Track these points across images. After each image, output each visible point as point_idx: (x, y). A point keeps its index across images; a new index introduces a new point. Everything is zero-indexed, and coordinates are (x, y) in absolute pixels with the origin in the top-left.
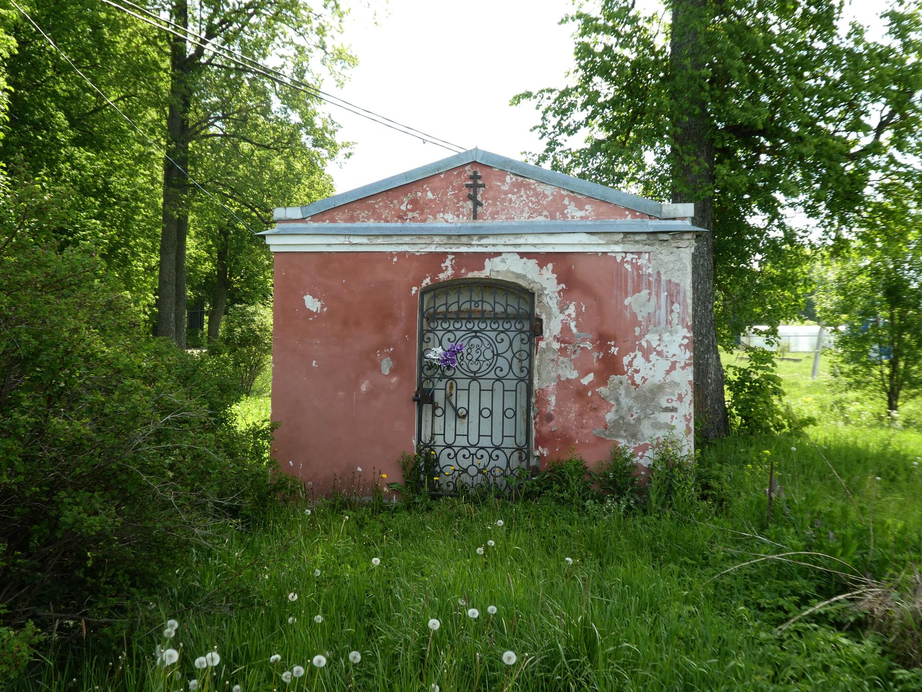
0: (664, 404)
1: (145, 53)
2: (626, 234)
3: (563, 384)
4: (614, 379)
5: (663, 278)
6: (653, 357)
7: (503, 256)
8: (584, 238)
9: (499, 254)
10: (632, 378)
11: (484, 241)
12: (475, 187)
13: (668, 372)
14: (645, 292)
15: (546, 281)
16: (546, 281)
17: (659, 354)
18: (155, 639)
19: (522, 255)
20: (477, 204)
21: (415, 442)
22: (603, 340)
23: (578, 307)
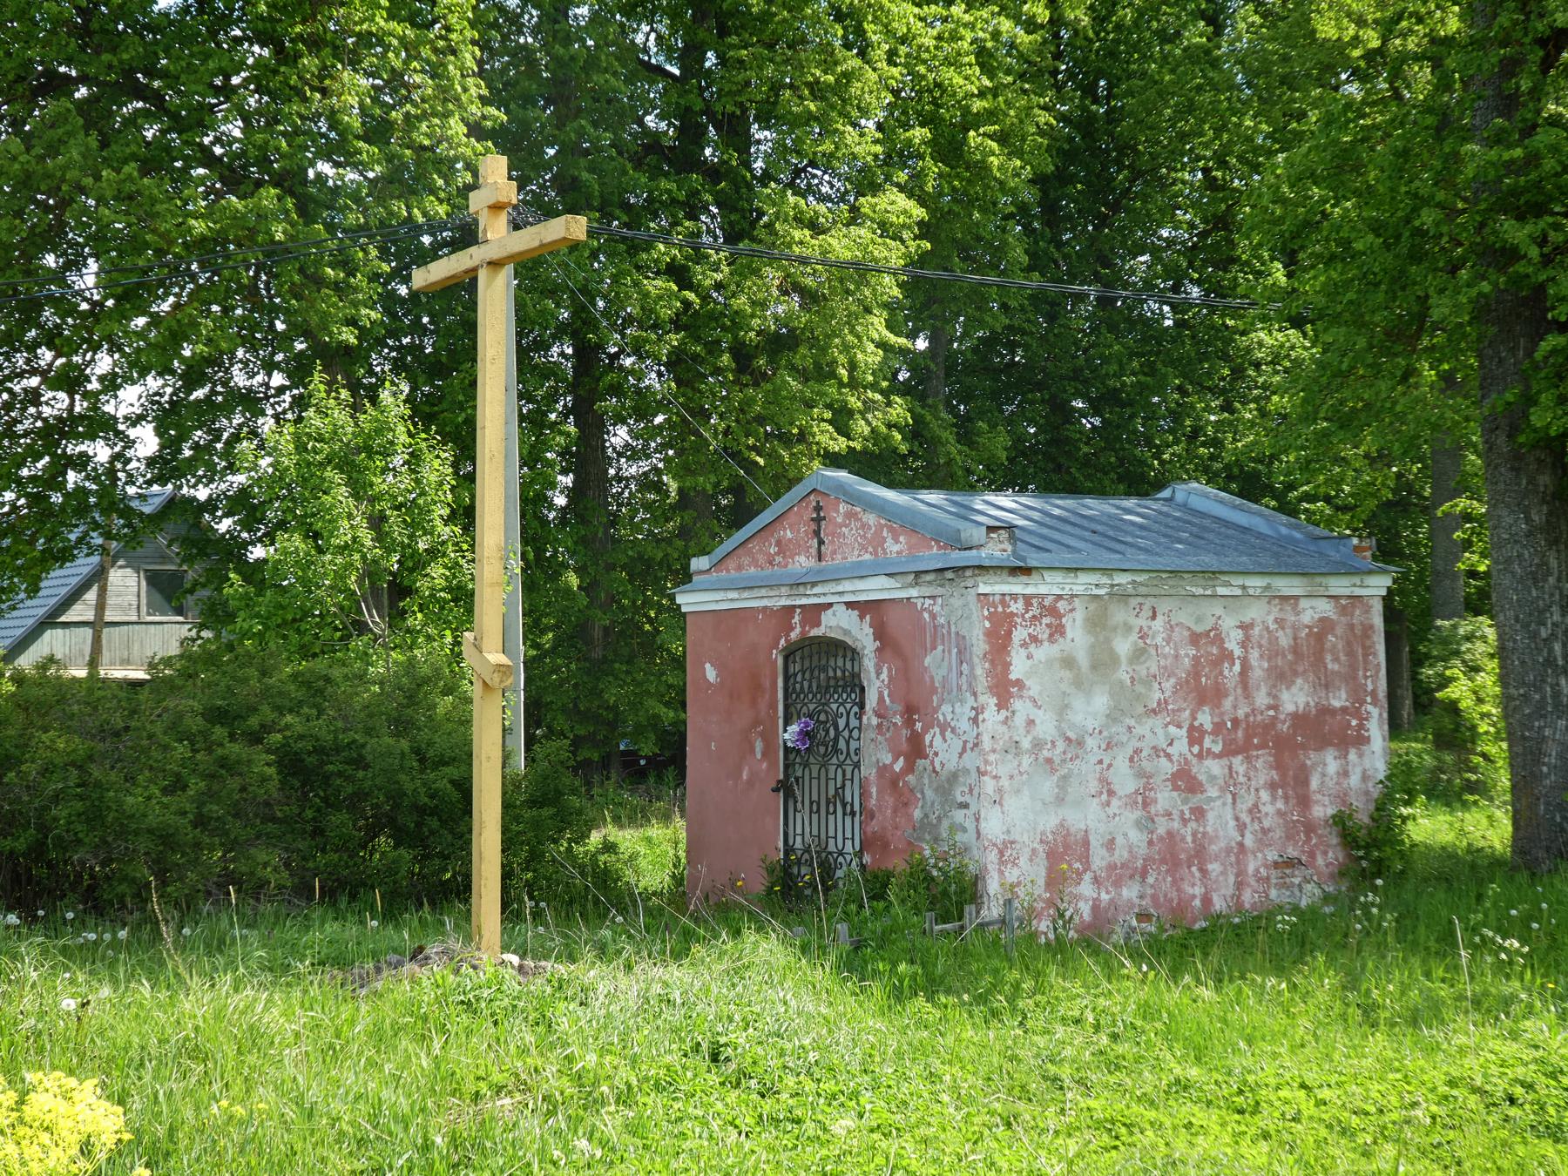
0: (960, 799)
1: (874, 174)
2: (918, 574)
3: (883, 770)
4: (921, 763)
5: (953, 629)
6: (948, 734)
7: (835, 607)
8: (883, 582)
9: (830, 605)
10: (932, 762)
11: (816, 590)
12: (818, 520)
13: (961, 755)
14: (940, 648)
15: (861, 635)
16: (861, 635)
17: (953, 731)
18: (165, 676)
19: (849, 605)
20: (821, 542)
21: (781, 844)
22: (910, 711)
23: (890, 670)
